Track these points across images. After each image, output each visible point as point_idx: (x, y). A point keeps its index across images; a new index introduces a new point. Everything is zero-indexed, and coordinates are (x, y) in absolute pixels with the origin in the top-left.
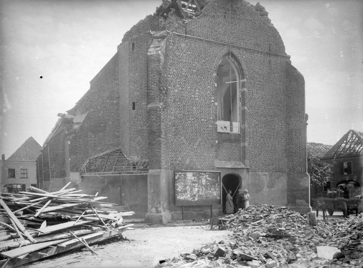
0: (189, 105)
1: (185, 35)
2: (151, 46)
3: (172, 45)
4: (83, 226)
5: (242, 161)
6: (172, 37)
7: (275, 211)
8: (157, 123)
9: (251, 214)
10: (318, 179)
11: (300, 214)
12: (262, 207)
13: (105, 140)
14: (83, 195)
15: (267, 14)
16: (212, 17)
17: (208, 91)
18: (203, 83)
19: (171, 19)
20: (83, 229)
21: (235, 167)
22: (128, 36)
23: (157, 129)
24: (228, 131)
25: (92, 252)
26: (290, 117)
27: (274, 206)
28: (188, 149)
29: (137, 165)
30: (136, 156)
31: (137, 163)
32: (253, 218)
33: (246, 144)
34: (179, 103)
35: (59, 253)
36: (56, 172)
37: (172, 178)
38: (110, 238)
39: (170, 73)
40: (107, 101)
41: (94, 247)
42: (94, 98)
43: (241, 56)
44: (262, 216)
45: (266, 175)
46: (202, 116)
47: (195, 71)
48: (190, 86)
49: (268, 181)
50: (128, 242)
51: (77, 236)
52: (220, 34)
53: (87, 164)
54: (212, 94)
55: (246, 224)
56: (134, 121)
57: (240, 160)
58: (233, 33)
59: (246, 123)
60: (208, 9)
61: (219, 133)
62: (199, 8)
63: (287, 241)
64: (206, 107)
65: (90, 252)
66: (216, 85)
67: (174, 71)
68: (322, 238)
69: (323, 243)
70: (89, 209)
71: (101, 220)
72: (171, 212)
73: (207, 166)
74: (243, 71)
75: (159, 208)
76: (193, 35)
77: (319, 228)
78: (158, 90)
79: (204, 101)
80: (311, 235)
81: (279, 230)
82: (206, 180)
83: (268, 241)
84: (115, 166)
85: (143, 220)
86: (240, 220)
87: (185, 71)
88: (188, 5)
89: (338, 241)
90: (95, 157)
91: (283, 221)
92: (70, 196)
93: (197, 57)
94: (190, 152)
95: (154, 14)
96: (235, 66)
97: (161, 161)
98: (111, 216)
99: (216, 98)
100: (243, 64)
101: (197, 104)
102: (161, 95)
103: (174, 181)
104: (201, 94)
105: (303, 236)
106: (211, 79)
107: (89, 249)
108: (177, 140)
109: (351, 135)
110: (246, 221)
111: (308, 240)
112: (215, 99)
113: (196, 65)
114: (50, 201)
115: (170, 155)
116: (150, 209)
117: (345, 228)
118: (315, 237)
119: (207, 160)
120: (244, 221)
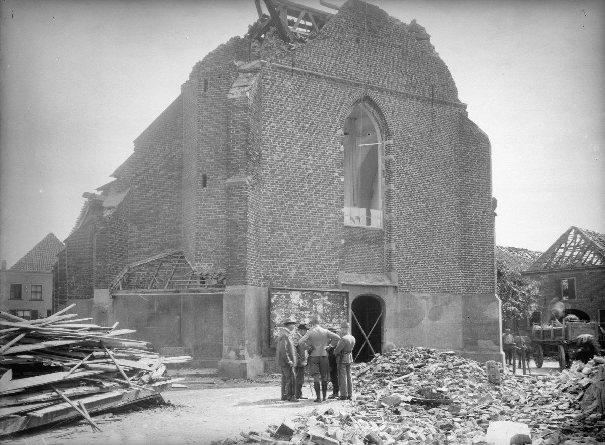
0: (297, 180)
1: (291, 67)
2: (234, 85)
5: (386, 274)
6: (270, 70)
7: (436, 359)
8: (240, 209)
9: (394, 363)
10: (518, 306)
12: (414, 352)
13: (155, 236)
14: (88, 326)
15: (427, 37)
16: (336, 41)
17: (328, 158)
19: (270, 43)
20: (83, 385)
22: (200, 68)
24: (363, 224)
25: (93, 427)
26: (467, 203)
27: (434, 350)
28: (294, 253)
29: (208, 278)
30: (207, 264)
31: (207, 275)
32: (396, 370)
33: (393, 246)
34: (280, 177)
35: (30, 427)
36: (78, 288)
37: (265, 300)
38: (137, 401)
39: (266, 129)
40: (162, 172)
41: (104, 418)
43: (384, 103)
44: (412, 366)
45: (427, 299)
47: (307, 125)
49: (430, 308)
51: (68, 397)
53: (124, 275)
54: (336, 163)
55: (385, 380)
57: (383, 273)
59: (393, 211)
60: (331, 28)
61: (348, 227)
63: (446, 411)
64: (326, 185)
65: (90, 426)
66: (342, 149)
67: (273, 124)
68: (506, 406)
69: (506, 416)
70: (100, 350)
71: (119, 371)
72: (264, 358)
73: (327, 281)
76: (305, 69)
77: (504, 389)
80: (488, 401)
81: (438, 391)
82: (324, 305)
83: (413, 411)
84: (171, 280)
85: (215, 371)
87: (291, 126)
88: (299, 21)
89: (533, 413)
91: (448, 376)
92: (65, 328)
93: (311, 104)
95: (245, 36)
96: (375, 118)
97: (246, 272)
98: (141, 365)
99: (343, 171)
102: (248, 163)
103: (270, 306)
104: (317, 163)
106: (335, 139)
107: (89, 421)
108: (275, 238)
109: (573, 235)
110: (385, 375)
111: (481, 410)
112: (341, 172)
113: (309, 116)
114: (22, 336)
116: (227, 352)
117: (550, 389)
119: (325, 272)
120: (381, 375)
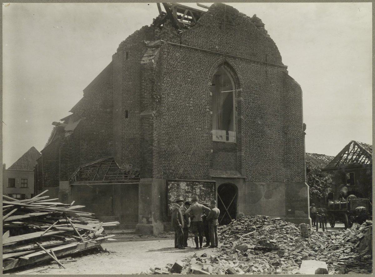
1: (179, 44)
2: (145, 55)
3: (167, 54)
4: (55, 237)
7: (269, 222)
10: (319, 190)
11: (295, 225)
18: (198, 92)
21: (231, 177)
23: (149, 138)
24: (224, 140)
25: (60, 265)
30: (128, 165)
32: (245, 230)
37: (164, 187)
39: (164, 82)
42: (87, 107)
43: (237, 66)
44: (254, 227)
45: (263, 185)
46: (197, 124)
47: (189, 80)
48: (184, 95)
50: (108, 254)
52: (215, 44)
53: (78, 173)
55: (238, 235)
56: (127, 129)
58: (228, 43)
59: (242, 132)
62: (195, 20)
63: (276, 254)
64: (201, 116)
66: (211, 94)
67: (168, 79)
71: (75, 231)
73: (202, 175)
74: (239, 80)
75: (150, 218)
76: (188, 45)
77: (311, 240)
78: (151, 98)
79: (199, 110)
80: (301, 248)
81: (270, 242)
82: (201, 189)
83: (255, 254)
84: (106, 175)
85: (134, 231)
86: (232, 232)
88: (184, 16)
89: (329, 255)
90: (87, 165)
94: (184, 161)
98: (89, 227)
100: (239, 73)
101: (192, 112)
103: (167, 191)
104: (196, 103)
105: (292, 249)
106: (206, 88)
107: (57, 262)
109: (353, 146)
110: (238, 233)
114: (15, 210)
115: (163, 164)
118: (306, 251)
